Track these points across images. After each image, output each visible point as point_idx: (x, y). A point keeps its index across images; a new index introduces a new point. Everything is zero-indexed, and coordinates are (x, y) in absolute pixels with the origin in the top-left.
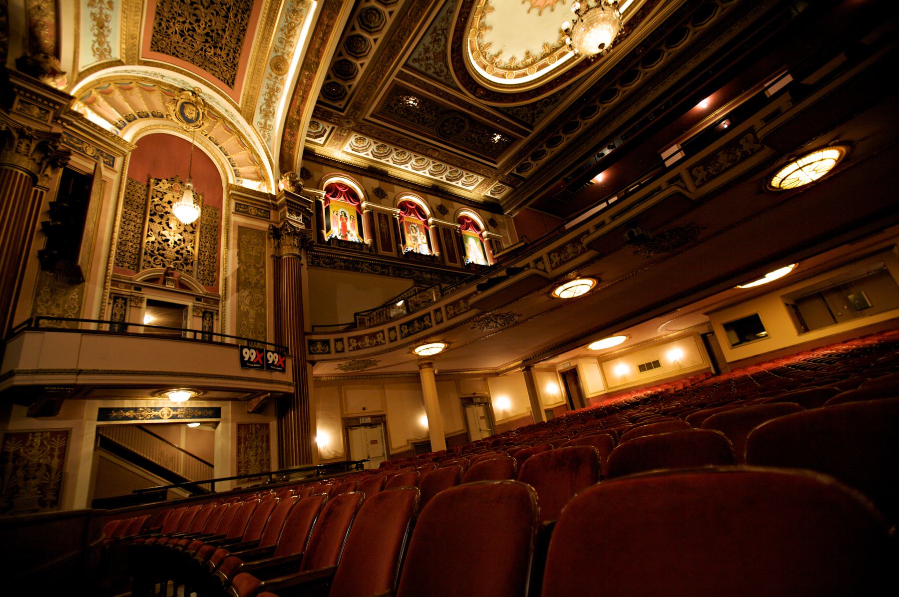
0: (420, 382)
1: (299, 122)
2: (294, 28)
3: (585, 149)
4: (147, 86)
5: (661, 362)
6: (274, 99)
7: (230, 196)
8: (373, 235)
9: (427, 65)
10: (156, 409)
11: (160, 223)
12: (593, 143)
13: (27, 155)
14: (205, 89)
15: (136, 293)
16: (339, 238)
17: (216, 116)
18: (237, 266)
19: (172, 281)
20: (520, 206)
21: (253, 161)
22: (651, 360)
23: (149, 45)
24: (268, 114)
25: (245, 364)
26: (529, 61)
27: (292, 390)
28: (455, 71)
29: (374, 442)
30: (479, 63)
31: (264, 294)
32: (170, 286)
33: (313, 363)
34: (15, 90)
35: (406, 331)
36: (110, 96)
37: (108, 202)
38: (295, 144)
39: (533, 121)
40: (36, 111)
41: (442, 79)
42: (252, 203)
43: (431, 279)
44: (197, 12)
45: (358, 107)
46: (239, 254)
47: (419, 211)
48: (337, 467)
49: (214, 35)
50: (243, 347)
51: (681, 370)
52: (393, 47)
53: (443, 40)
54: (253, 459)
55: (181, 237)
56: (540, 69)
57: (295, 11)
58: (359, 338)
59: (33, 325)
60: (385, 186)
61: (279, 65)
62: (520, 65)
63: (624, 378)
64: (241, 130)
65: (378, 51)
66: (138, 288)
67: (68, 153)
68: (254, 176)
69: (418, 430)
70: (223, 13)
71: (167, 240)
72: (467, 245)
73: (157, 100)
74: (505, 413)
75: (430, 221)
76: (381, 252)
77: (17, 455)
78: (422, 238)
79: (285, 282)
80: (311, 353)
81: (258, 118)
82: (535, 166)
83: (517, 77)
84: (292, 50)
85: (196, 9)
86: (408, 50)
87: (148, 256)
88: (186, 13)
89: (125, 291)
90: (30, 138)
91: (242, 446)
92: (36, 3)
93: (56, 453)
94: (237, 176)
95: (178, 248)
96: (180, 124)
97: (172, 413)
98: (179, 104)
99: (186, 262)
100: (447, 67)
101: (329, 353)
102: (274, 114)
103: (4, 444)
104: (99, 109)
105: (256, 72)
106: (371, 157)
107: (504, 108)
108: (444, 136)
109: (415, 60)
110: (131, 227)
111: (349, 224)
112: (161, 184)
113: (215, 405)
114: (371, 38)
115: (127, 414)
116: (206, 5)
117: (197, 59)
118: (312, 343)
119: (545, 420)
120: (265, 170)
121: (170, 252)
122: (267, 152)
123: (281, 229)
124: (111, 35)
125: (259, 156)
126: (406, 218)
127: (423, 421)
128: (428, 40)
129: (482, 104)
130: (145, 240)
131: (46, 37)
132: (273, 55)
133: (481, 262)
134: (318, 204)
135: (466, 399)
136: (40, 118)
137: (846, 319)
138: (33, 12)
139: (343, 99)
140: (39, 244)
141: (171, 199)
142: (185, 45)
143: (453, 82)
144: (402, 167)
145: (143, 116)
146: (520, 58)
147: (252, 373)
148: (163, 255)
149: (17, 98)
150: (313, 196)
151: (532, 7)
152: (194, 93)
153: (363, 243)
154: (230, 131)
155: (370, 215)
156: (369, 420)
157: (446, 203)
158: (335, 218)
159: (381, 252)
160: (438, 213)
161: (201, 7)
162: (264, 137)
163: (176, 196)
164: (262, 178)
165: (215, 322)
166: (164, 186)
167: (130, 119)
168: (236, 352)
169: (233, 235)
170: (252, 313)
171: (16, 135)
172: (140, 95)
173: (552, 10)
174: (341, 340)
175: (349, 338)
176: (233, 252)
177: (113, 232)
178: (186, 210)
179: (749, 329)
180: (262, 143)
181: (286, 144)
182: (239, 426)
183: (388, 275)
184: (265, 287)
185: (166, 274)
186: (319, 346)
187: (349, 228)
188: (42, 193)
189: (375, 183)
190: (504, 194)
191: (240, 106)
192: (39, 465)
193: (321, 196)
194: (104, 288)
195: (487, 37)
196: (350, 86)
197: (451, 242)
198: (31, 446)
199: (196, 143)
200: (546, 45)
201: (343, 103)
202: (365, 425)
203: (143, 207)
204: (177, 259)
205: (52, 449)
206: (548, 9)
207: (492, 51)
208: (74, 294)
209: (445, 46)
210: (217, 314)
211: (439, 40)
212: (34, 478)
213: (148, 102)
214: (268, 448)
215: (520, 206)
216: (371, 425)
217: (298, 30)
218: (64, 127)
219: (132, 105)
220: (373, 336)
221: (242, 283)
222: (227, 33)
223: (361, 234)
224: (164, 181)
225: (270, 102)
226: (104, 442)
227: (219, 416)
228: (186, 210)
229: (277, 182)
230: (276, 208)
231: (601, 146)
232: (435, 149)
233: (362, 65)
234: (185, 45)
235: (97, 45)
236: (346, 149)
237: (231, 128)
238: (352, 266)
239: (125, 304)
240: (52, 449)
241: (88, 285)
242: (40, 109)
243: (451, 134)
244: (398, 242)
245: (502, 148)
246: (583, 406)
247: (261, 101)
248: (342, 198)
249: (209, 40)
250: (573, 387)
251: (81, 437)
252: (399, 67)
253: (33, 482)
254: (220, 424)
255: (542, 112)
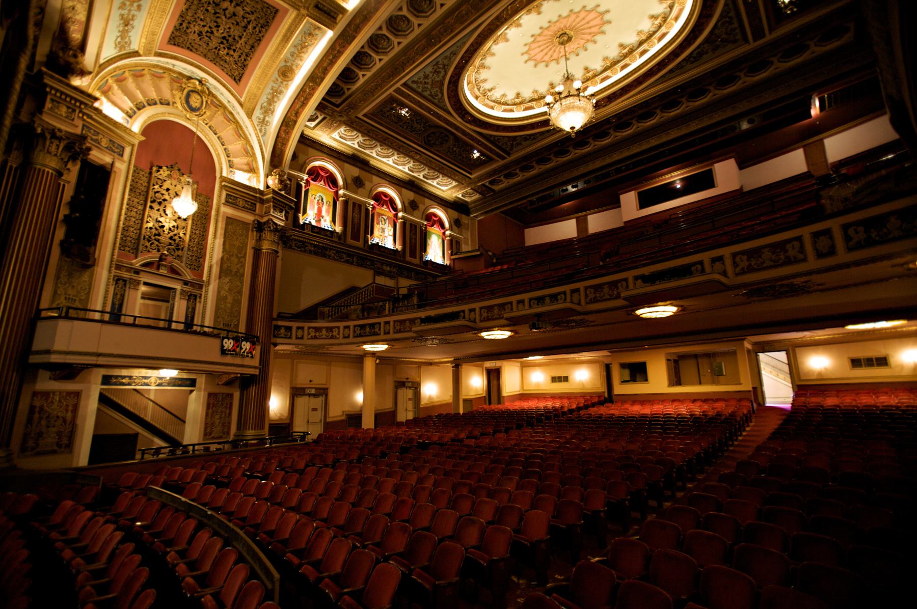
0: (362, 363)
1: (295, 122)
2: (306, 47)
3: (552, 182)
4: (159, 73)
5: (570, 379)
6: (275, 99)
7: (222, 187)
8: (344, 224)
9: (424, 88)
10: (146, 378)
11: (158, 210)
12: (561, 179)
13: (56, 155)
14: (211, 81)
15: (135, 276)
16: (314, 223)
17: (221, 106)
18: (220, 256)
19: (165, 266)
20: (486, 212)
21: (247, 152)
22: (563, 374)
23: (167, 39)
24: (268, 110)
25: (223, 352)
26: (518, 101)
27: (256, 372)
28: (449, 98)
29: (315, 410)
30: (473, 93)
31: (242, 283)
32: (163, 271)
33: (276, 345)
34: (48, 89)
35: (358, 332)
36: (124, 83)
37: (117, 192)
38: (288, 140)
39: (512, 149)
40: (63, 110)
41: (436, 101)
42: (241, 196)
43: (390, 272)
44: (219, 20)
45: (353, 107)
46: (224, 244)
47: (392, 203)
48: (282, 429)
49: (231, 39)
50: (224, 338)
51: (583, 388)
52: (396, 69)
53: (443, 73)
54: (217, 422)
55: (175, 224)
56: (526, 109)
57: (310, 34)
58: (318, 329)
59: (63, 315)
60: (364, 175)
61: (286, 73)
62: (510, 102)
63: (538, 384)
64: (240, 121)
65: (381, 68)
66: (137, 272)
67: (89, 149)
68: (246, 167)
69: (353, 404)
70: (243, 24)
71: (163, 227)
72: (429, 242)
73: (165, 85)
74: (430, 398)
75: (400, 214)
76: (349, 242)
77: (42, 409)
78: (389, 231)
79: (262, 273)
80: (275, 336)
81: (258, 113)
82: (505, 184)
83: (505, 111)
84: (301, 63)
85: (218, 17)
86: (410, 74)
87: (146, 241)
88: (208, 20)
89: (126, 275)
90: (60, 139)
91: (210, 411)
92: (71, 4)
93: (70, 408)
94: (231, 167)
95: (172, 234)
96: (185, 112)
97: (159, 381)
98: (185, 92)
99: (178, 248)
100: (442, 94)
101: (290, 338)
102: (273, 112)
103: (33, 399)
104: (114, 98)
105: (264, 73)
106: (356, 146)
107: (491, 136)
108: (428, 145)
109: (414, 82)
110: (133, 214)
111: (324, 209)
112: (161, 172)
113: (192, 376)
114: (376, 57)
115: (124, 381)
116: (228, 16)
117: (209, 55)
118: (278, 328)
119: (461, 412)
120: (256, 162)
121: (164, 239)
122: (261, 146)
123: (265, 223)
124: (134, 31)
125: (252, 148)
126: (378, 209)
127: (359, 397)
128: (430, 69)
129: (469, 128)
130: (145, 226)
131: (76, 35)
132: (283, 64)
133: (438, 260)
134: (299, 187)
135: (399, 382)
136: (66, 117)
137: (707, 383)
138: (67, 10)
139: (340, 96)
140: (60, 234)
141: (170, 187)
142: (200, 43)
143: (445, 105)
144: (385, 160)
145: (151, 103)
146: (510, 96)
147: (228, 359)
148: (158, 240)
149: (49, 97)
150: (297, 177)
151: (529, 59)
152: (200, 82)
153: (334, 231)
154: (229, 120)
155: (346, 203)
156: (313, 391)
157: (418, 198)
158: (312, 202)
159: (350, 241)
160: (409, 209)
161: (223, 17)
162: (261, 131)
163: (174, 183)
164: (252, 170)
165: (198, 304)
166: (164, 173)
167: (140, 107)
168: (217, 342)
169: (221, 225)
170: (230, 299)
171: (49, 137)
172: (150, 82)
173: (547, 66)
174: (302, 328)
175: (309, 328)
176: (219, 241)
177: (119, 220)
178: (184, 205)
179: (638, 372)
180: (258, 137)
181: (280, 139)
182: (210, 395)
183: (352, 263)
184: (243, 275)
185: (161, 259)
186: (283, 331)
187: (324, 213)
188: (64, 186)
189: (355, 171)
190: (473, 198)
191: (242, 100)
192: (58, 417)
193: (302, 179)
194: (110, 271)
195: (484, 74)
196: (348, 89)
197: (414, 238)
198: (52, 402)
199: (199, 134)
200: (535, 91)
201: (339, 101)
202: (309, 395)
203: (146, 195)
204: (170, 244)
205: (67, 406)
206: (544, 64)
207: (487, 86)
208: (85, 277)
209: (444, 77)
210: (200, 297)
211: (439, 72)
212: (54, 426)
213: (158, 90)
214: (230, 414)
215: (486, 212)
216: (315, 395)
217: (310, 49)
218: (84, 120)
219: (143, 93)
220: (330, 329)
221: (225, 270)
222: (243, 39)
223: (334, 221)
224: (164, 168)
225: (272, 101)
226: (104, 399)
227: (194, 386)
228: (184, 205)
229: (267, 176)
230: (262, 202)
231: (567, 182)
232: (418, 152)
233: (363, 77)
234: (200, 43)
235: (119, 40)
236: (333, 137)
237: (231, 118)
238: (321, 251)
239: (125, 285)
240: (67, 406)
241: (98, 269)
242: (68, 108)
243: (434, 144)
244: (366, 233)
245: (478, 163)
246: (499, 403)
247: (263, 99)
248: (322, 182)
249: (225, 42)
250: (494, 382)
251: (88, 396)
252: (398, 85)
253: (54, 430)
254: (194, 393)
255: (520, 144)
